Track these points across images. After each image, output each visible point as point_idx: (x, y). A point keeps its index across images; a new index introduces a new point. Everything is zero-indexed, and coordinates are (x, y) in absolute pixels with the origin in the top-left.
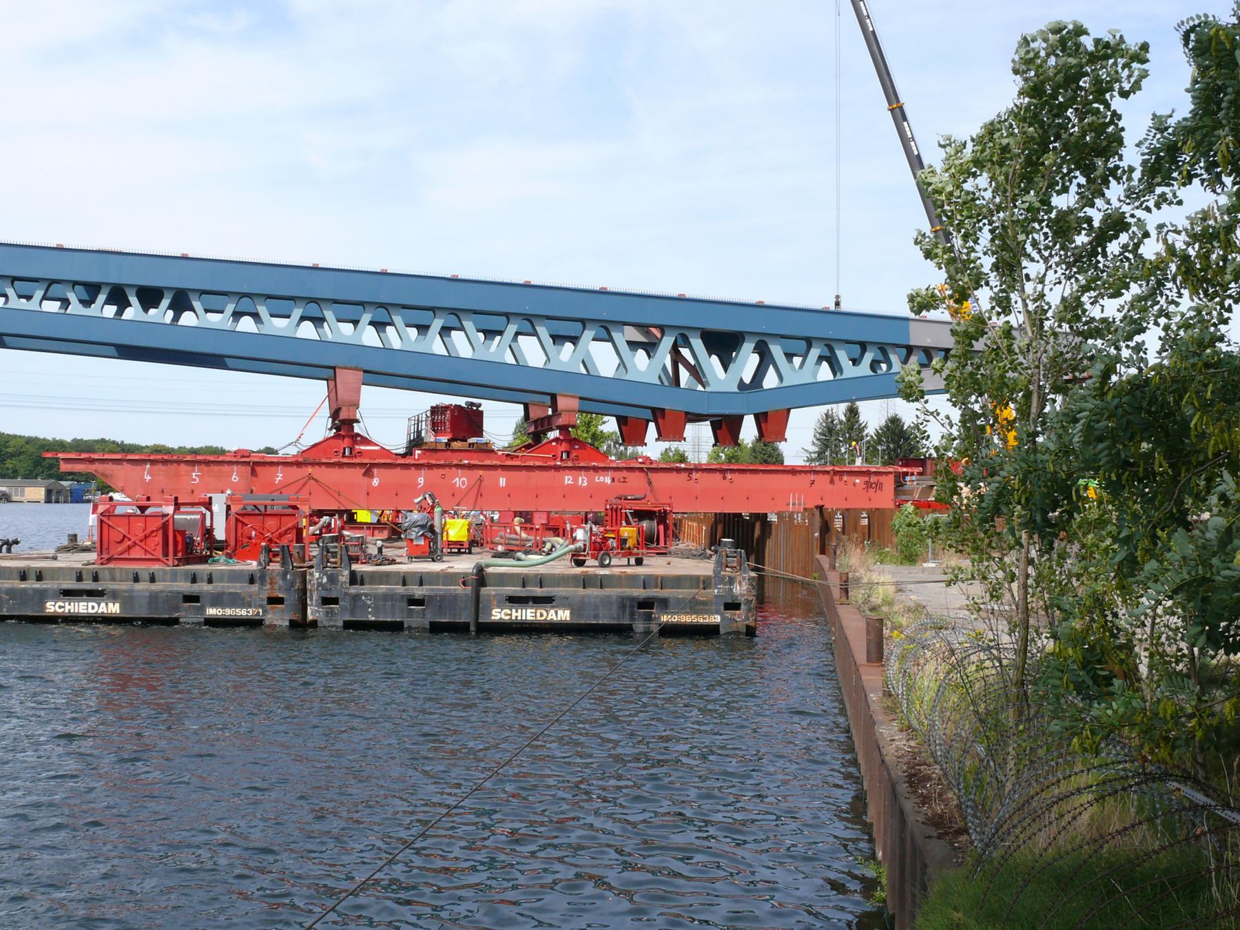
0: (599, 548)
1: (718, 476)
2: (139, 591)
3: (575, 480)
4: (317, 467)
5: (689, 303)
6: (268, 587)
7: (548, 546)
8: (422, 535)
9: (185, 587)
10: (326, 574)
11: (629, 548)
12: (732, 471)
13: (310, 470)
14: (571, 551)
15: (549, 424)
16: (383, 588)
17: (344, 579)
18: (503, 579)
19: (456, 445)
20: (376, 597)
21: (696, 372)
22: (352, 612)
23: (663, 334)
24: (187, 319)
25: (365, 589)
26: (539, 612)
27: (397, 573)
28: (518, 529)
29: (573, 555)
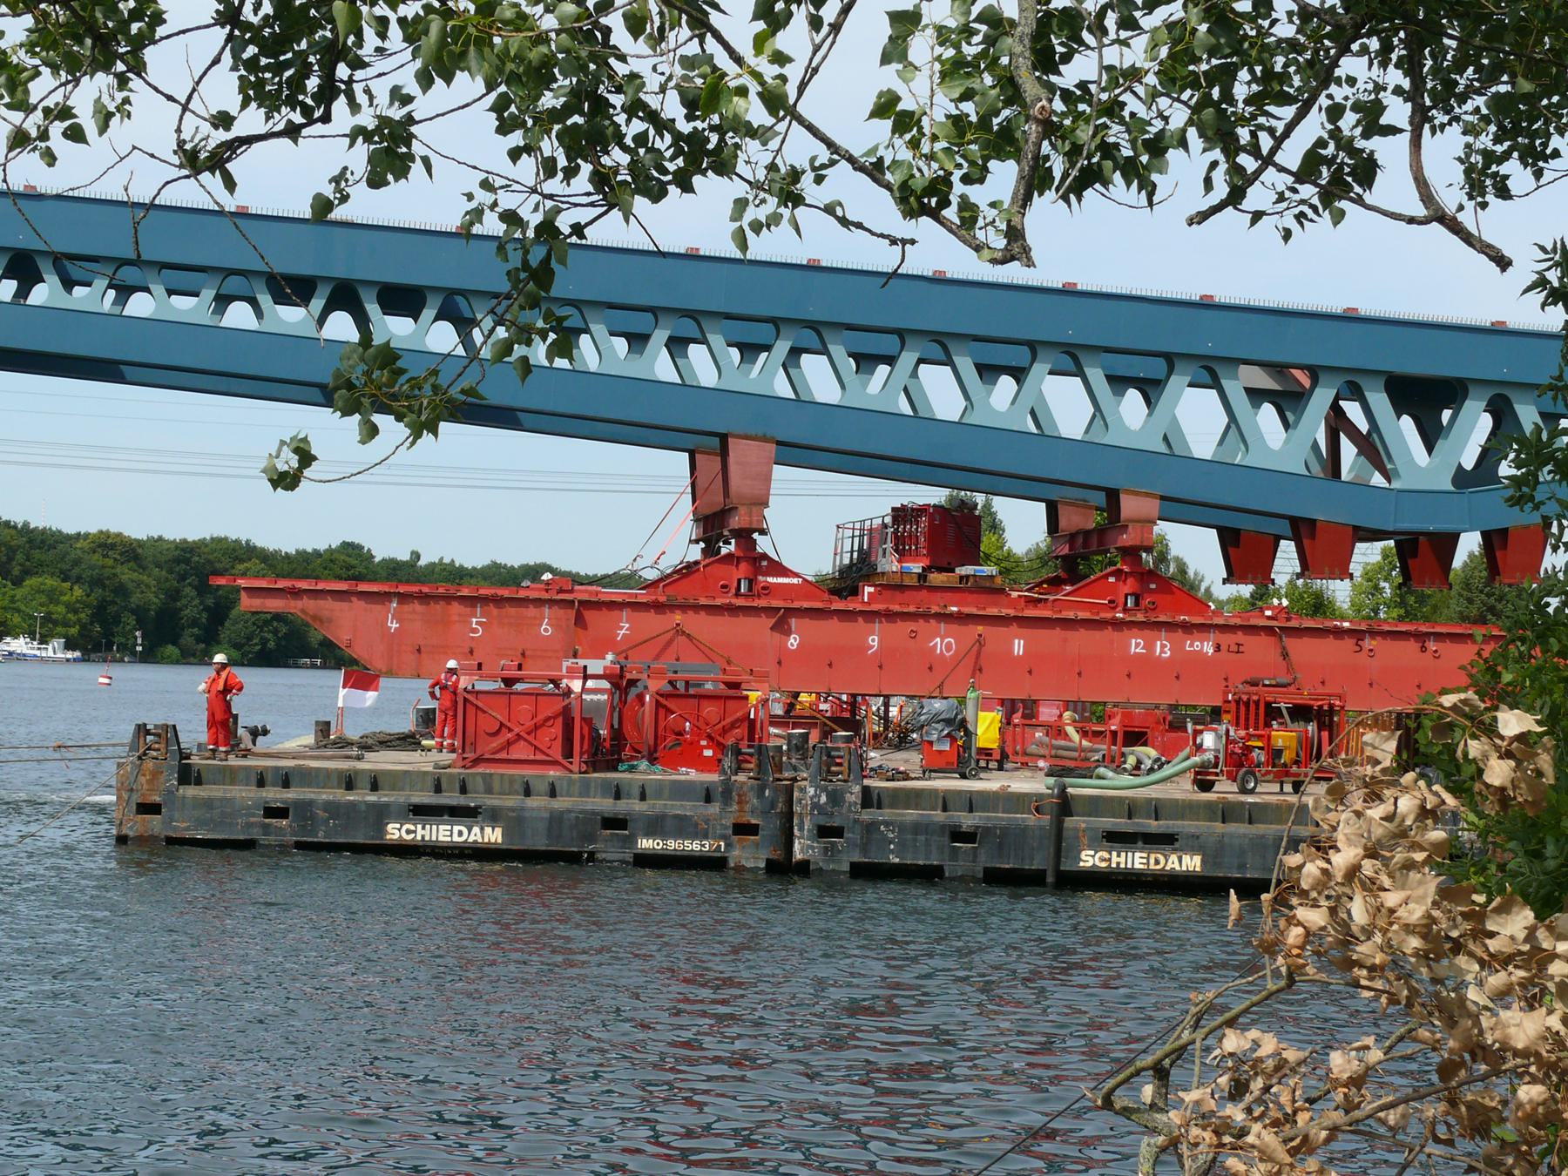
0: (1237, 762)
1: (1412, 646)
2: (533, 809)
3: (1150, 646)
4: (691, 613)
5: (1513, 339)
6: (735, 807)
7: (1131, 761)
8: (948, 735)
9: (606, 805)
10: (825, 789)
11: (1285, 765)
12: (1439, 637)
13: (678, 617)
14: (1195, 766)
15: (1101, 543)
16: (911, 814)
17: (853, 798)
18: (1096, 806)
19: (937, 578)
20: (902, 828)
21: (1373, 449)
22: (865, 850)
23: (1315, 383)
24: (140, 306)
25: (886, 814)
26: (1153, 856)
27: (934, 792)
28: (1070, 730)
29: (1197, 773)
